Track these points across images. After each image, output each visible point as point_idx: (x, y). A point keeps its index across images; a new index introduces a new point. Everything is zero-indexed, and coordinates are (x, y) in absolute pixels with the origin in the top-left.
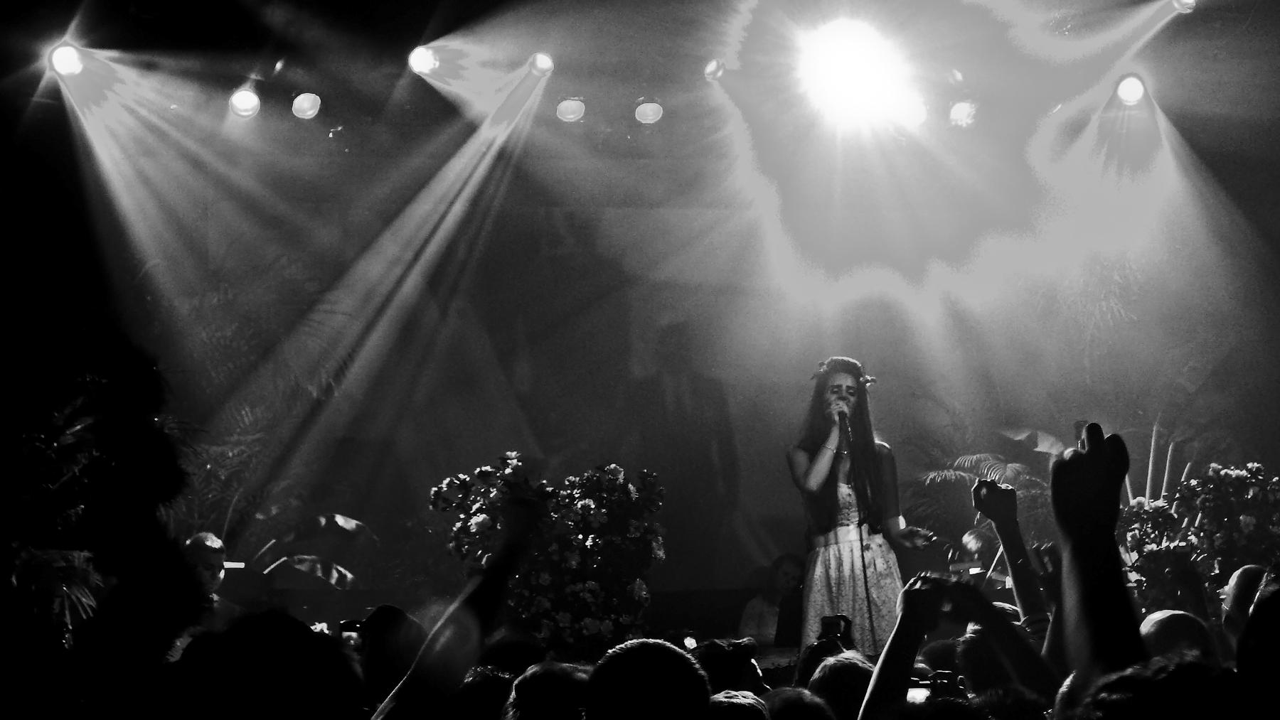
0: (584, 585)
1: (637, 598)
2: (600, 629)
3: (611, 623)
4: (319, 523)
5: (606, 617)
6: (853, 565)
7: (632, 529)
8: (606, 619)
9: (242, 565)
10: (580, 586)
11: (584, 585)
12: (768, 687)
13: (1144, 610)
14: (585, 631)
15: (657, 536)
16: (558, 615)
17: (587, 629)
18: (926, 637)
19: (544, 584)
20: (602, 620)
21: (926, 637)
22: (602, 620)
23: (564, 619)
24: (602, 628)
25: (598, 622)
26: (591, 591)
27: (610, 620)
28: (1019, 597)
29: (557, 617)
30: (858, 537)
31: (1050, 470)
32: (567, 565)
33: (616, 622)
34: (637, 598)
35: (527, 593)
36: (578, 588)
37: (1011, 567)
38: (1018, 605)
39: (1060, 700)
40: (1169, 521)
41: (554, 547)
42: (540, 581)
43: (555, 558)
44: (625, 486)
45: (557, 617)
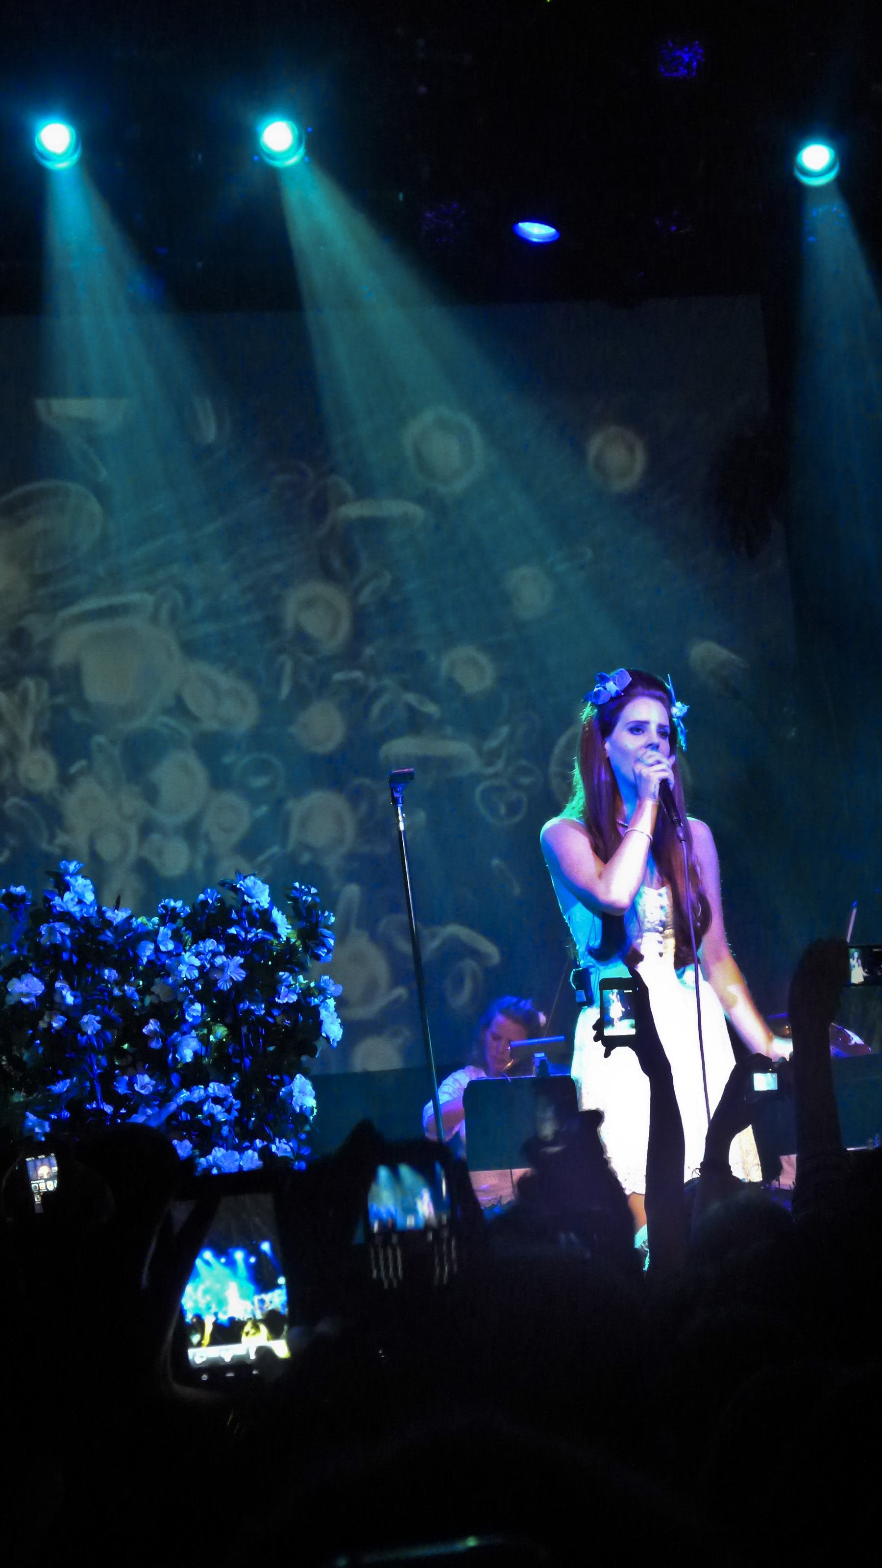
0: (206, 1089)
1: (298, 1109)
3: (256, 1155)
5: (247, 1144)
6: (50, 1163)
7: (283, 990)
8: (247, 1148)
9: (631, 991)
10: (199, 1092)
11: (206, 1089)
19: (142, 1092)
22: (241, 1150)
25: (237, 1155)
28: (672, 682)
30: (694, 979)
31: (656, 675)
34: (298, 1109)
35: (108, 1109)
36: (196, 1095)
37: (855, 1150)
38: (671, 684)
39: (659, 794)
41: (152, 1026)
42: (137, 1088)
43: (155, 1045)
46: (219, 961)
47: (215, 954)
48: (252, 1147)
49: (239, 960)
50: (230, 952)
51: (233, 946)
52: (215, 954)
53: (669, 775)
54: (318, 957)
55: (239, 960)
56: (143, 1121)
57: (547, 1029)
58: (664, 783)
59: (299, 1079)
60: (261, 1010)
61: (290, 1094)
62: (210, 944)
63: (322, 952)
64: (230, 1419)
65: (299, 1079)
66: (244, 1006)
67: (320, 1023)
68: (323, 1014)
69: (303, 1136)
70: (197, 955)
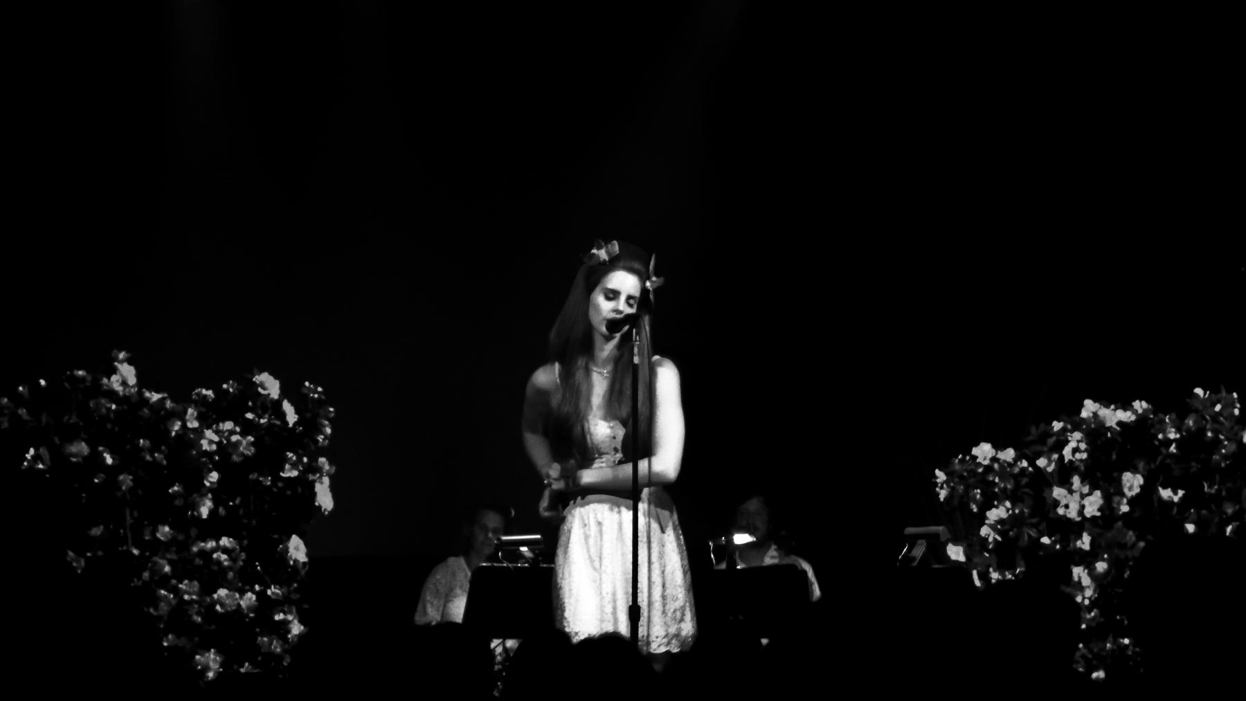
1: (292, 563)
2: (239, 605)
3: (254, 597)
4: (258, 657)
10: (211, 544)
12: (712, 556)
13: (1224, 516)
14: (218, 608)
15: (321, 476)
16: (181, 583)
17: (222, 606)
18: (1114, 457)
20: (242, 593)
21: (1114, 457)
23: (189, 590)
24: (242, 603)
26: (225, 550)
27: (254, 592)
29: (180, 586)
32: (196, 513)
33: (261, 596)
34: (292, 563)
40: (972, 480)
44: (278, 404)
45: (180, 586)
47: (232, 432)
50: (244, 434)
51: (247, 428)
62: (228, 425)
68: (318, 487)
70: (217, 432)
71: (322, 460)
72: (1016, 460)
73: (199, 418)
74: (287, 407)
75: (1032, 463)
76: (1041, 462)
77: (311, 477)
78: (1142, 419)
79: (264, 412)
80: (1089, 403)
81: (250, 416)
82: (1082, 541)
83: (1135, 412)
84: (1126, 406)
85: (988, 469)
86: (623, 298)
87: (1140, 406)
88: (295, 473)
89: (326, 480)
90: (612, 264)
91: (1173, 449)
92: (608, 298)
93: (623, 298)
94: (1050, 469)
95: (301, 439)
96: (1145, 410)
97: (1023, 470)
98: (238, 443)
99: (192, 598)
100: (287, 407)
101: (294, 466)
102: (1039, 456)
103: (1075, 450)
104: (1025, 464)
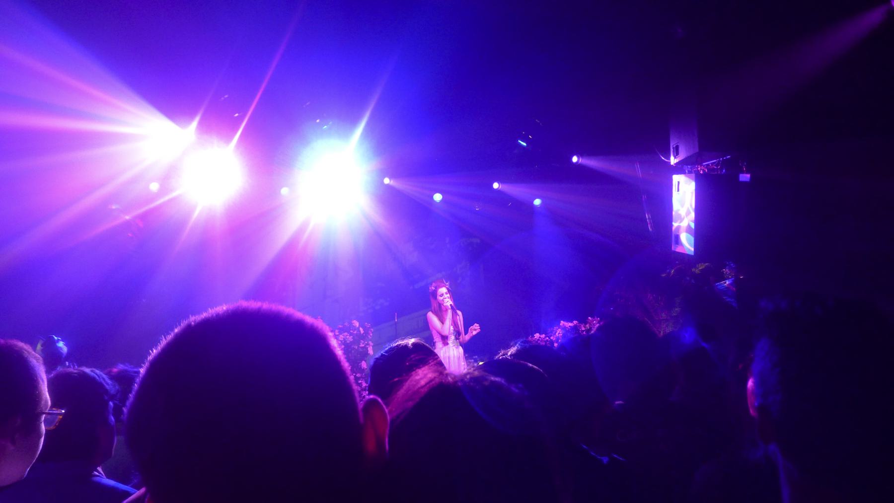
7: (361, 344)
44: (359, 328)
46: (348, 337)
47: (347, 335)
48: (353, 375)
49: (352, 337)
50: (350, 335)
51: (351, 334)
52: (347, 335)
53: (451, 303)
54: (368, 337)
55: (352, 337)
56: (692, 235)
57: (435, 361)
58: (451, 305)
59: (363, 362)
60: (356, 347)
61: (361, 365)
62: (346, 334)
63: (369, 336)
64: (594, 454)
65: (363, 362)
66: (353, 346)
67: (368, 351)
68: (369, 349)
69: (588, 326)
70: (343, 335)
71: (370, 342)
72: (545, 337)
73: (339, 332)
74: (361, 329)
75: (549, 338)
76: (552, 338)
77: (367, 346)
78: (575, 326)
79: (355, 330)
80: (562, 322)
81: (351, 331)
82: (443, 347)
83: (574, 323)
84: (572, 322)
85: (538, 340)
86: (445, 294)
87: (575, 322)
88: (363, 346)
89: (371, 347)
90: (437, 288)
91: (584, 333)
92: (441, 297)
93: (445, 294)
94: (554, 339)
95: (363, 337)
96: (577, 323)
97: (547, 340)
98: (348, 338)
99: (446, 310)
100: (361, 329)
101: (363, 344)
102: (551, 336)
103: (559, 333)
104: (548, 338)
